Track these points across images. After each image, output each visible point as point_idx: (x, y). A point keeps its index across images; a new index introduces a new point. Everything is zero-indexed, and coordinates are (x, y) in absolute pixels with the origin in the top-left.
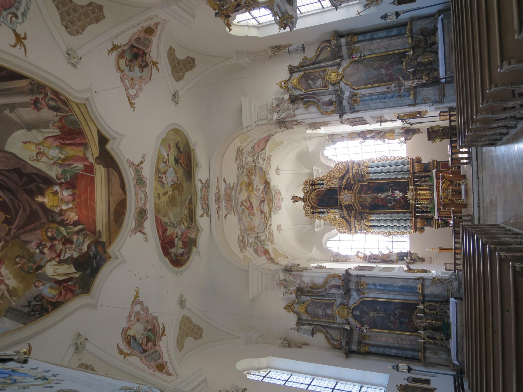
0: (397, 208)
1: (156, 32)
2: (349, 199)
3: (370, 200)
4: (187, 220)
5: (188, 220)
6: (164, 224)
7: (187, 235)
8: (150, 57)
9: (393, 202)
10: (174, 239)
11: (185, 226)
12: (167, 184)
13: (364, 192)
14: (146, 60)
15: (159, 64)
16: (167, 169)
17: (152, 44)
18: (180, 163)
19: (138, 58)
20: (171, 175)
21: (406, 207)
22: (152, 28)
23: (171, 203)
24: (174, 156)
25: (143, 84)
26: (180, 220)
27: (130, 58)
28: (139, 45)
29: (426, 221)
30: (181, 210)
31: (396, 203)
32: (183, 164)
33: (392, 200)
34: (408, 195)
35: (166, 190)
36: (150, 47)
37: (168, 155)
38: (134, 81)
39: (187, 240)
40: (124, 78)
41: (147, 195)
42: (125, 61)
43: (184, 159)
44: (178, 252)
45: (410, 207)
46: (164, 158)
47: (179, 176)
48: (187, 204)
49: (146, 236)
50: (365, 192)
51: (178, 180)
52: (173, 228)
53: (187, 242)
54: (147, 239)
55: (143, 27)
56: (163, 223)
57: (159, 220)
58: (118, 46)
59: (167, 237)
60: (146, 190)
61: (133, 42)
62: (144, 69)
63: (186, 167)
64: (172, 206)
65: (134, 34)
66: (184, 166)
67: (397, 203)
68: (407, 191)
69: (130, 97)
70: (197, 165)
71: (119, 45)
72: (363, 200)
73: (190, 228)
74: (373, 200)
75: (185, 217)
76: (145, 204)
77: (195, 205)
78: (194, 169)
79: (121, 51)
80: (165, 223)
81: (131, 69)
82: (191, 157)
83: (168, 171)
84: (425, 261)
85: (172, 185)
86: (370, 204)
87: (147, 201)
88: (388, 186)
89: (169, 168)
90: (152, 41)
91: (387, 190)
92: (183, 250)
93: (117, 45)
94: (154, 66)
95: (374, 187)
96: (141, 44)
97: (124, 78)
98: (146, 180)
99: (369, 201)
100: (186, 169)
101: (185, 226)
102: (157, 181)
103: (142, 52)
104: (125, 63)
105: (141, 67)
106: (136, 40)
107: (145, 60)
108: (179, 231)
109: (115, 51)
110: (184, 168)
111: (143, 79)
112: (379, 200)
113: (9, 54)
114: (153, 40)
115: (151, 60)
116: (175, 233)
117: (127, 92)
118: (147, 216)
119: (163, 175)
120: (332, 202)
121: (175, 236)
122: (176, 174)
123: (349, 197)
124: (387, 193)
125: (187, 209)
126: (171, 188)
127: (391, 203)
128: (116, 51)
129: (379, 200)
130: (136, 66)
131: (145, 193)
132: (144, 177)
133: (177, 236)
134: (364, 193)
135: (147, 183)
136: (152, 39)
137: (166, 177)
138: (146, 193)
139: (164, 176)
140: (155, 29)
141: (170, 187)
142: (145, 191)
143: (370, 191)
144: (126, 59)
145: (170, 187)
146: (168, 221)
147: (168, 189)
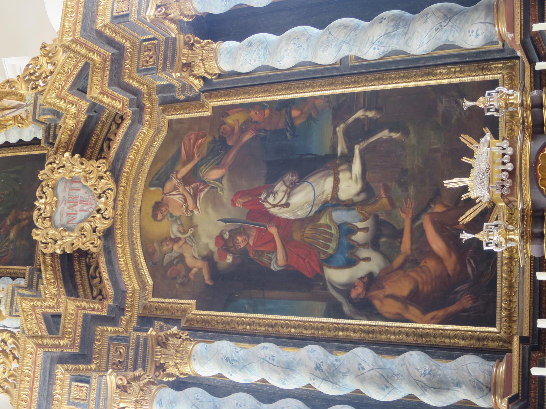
0: (391, 307)
2: (81, 215)
3: (216, 233)
9: (364, 253)
13: (184, 171)
21: (466, 302)
29: (188, 216)
31: (388, 258)
33: (359, 237)
34: (466, 170)
45: (501, 303)
50: (194, 171)
67: (398, 261)
68: (465, 159)
72: (175, 231)
74: (233, 233)
86: (208, 259)
88: (340, 129)
91: (333, 156)
95: (247, 137)
99: (204, 240)
112: (273, 230)
120: (12, 235)
123: (84, 202)
124: (329, 183)
127: (351, 263)
129: (273, 230)
134: (186, 181)
143: (218, 166)
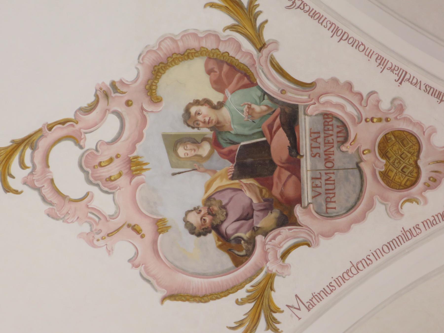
1: (410, 200)
8: (284, 255)
14: (259, 239)
15: (316, 10)
17: (346, 229)
19: (250, 181)
22: (421, 163)
25: (131, 253)
27: (236, 128)
28: (313, 156)
36: (328, 225)
38: (123, 181)
40: (122, 109)
42: (207, 102)
55: (401, 108)
58: (259, 32)
61: (310, 110)
62: (212, 237)
65: (349, 86)
69: (39, 154)
71: (267, 35)
79: (244, 61)
81: (181, 151)
84: (296, 295)
90: (363, 217)
93: (259, 21)
94: (249, 306)
96: (321, 166)
97: (122, 109)
103: (290, 192)
104: (197, 103)
105: (210, 213)
106: (327, 116)
107: (255, 231)
109: (229, 21)
111: (155, 242)
114: (371, 216)
115: (272, 267)
117: (58, 132)
128: (232, 28)
130: (208, 177)
136: (370, 206)
140: (424, 178)
144: (221, 105)
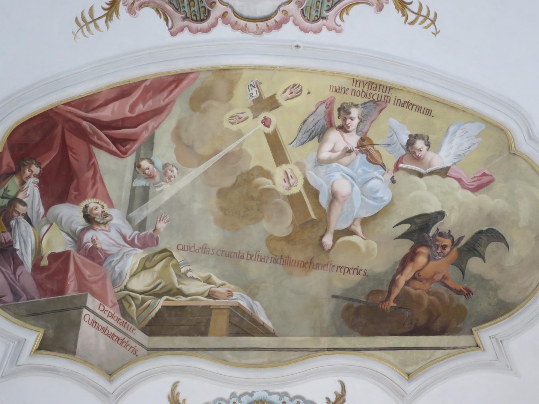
4: (159, 296)
5: (161, 302)
6: (145, 135)
7: (94, 294)
10: (77, 201)
11: (133, 276)
12: (320, 162)
16: (383, 166)
18: (411, 257)
20: (356, 188)
23: (235, 186)
24: (441, 215)
26: (162, 245)
30: (205, 250)
32: (409, 272)
35: (292, 152)
37: (444, 172)
39: (72, 289)
41: (269, 29)
43: (431, 279)
44: (23, 223)
46: (428, 145)
47: (353, 244)
48: (230, 294)
49: (101, 23)
51: (338, 234)
52: (126, 195)
53: (62, 291)
54: (87, 24)
56: (151, 124)
57: (160, 101)
59: (91, 156)
60: (290, 25)
63: (396, 292)
64: (222, 193)
66: (402, 280)
70: (409, 375)
73: (124, 313)
75: (175, 279)
76: (234, 19)
77: (228, 355)
78: (389, 355)
80: (150, 143)
82: (443, 332)
83: (377, 172)
85: (314, 193)
87: (244, 30)
89: (388, 176)
92: (28, 261)
98: (330, 29)
100: (390, 292)
101: (133, 276)
102: (328, 94)
108: (114, 234)
110: (393, 283)
113: (496, 109)
116: (107, 210)
118: (181, 30)
119: (358, 138)
121: (92, 203)
122: (365, 222)
125: (211, 295)
126: (298, 188)
131: (278, 17)
132: (345, 16)
133: (89, 218)
135: (318, 31)
137: (349, 152)
138: (278, 26)
139: (353, 140)
141: (306, 183)
142: (285, 21)
145: (306, 183)
146: (159, 163)
147: (298, 164)
